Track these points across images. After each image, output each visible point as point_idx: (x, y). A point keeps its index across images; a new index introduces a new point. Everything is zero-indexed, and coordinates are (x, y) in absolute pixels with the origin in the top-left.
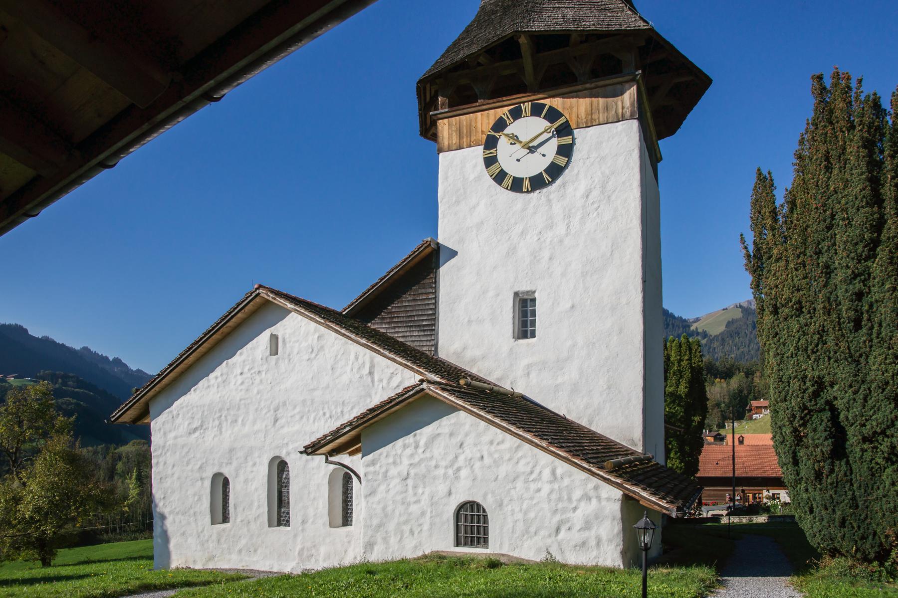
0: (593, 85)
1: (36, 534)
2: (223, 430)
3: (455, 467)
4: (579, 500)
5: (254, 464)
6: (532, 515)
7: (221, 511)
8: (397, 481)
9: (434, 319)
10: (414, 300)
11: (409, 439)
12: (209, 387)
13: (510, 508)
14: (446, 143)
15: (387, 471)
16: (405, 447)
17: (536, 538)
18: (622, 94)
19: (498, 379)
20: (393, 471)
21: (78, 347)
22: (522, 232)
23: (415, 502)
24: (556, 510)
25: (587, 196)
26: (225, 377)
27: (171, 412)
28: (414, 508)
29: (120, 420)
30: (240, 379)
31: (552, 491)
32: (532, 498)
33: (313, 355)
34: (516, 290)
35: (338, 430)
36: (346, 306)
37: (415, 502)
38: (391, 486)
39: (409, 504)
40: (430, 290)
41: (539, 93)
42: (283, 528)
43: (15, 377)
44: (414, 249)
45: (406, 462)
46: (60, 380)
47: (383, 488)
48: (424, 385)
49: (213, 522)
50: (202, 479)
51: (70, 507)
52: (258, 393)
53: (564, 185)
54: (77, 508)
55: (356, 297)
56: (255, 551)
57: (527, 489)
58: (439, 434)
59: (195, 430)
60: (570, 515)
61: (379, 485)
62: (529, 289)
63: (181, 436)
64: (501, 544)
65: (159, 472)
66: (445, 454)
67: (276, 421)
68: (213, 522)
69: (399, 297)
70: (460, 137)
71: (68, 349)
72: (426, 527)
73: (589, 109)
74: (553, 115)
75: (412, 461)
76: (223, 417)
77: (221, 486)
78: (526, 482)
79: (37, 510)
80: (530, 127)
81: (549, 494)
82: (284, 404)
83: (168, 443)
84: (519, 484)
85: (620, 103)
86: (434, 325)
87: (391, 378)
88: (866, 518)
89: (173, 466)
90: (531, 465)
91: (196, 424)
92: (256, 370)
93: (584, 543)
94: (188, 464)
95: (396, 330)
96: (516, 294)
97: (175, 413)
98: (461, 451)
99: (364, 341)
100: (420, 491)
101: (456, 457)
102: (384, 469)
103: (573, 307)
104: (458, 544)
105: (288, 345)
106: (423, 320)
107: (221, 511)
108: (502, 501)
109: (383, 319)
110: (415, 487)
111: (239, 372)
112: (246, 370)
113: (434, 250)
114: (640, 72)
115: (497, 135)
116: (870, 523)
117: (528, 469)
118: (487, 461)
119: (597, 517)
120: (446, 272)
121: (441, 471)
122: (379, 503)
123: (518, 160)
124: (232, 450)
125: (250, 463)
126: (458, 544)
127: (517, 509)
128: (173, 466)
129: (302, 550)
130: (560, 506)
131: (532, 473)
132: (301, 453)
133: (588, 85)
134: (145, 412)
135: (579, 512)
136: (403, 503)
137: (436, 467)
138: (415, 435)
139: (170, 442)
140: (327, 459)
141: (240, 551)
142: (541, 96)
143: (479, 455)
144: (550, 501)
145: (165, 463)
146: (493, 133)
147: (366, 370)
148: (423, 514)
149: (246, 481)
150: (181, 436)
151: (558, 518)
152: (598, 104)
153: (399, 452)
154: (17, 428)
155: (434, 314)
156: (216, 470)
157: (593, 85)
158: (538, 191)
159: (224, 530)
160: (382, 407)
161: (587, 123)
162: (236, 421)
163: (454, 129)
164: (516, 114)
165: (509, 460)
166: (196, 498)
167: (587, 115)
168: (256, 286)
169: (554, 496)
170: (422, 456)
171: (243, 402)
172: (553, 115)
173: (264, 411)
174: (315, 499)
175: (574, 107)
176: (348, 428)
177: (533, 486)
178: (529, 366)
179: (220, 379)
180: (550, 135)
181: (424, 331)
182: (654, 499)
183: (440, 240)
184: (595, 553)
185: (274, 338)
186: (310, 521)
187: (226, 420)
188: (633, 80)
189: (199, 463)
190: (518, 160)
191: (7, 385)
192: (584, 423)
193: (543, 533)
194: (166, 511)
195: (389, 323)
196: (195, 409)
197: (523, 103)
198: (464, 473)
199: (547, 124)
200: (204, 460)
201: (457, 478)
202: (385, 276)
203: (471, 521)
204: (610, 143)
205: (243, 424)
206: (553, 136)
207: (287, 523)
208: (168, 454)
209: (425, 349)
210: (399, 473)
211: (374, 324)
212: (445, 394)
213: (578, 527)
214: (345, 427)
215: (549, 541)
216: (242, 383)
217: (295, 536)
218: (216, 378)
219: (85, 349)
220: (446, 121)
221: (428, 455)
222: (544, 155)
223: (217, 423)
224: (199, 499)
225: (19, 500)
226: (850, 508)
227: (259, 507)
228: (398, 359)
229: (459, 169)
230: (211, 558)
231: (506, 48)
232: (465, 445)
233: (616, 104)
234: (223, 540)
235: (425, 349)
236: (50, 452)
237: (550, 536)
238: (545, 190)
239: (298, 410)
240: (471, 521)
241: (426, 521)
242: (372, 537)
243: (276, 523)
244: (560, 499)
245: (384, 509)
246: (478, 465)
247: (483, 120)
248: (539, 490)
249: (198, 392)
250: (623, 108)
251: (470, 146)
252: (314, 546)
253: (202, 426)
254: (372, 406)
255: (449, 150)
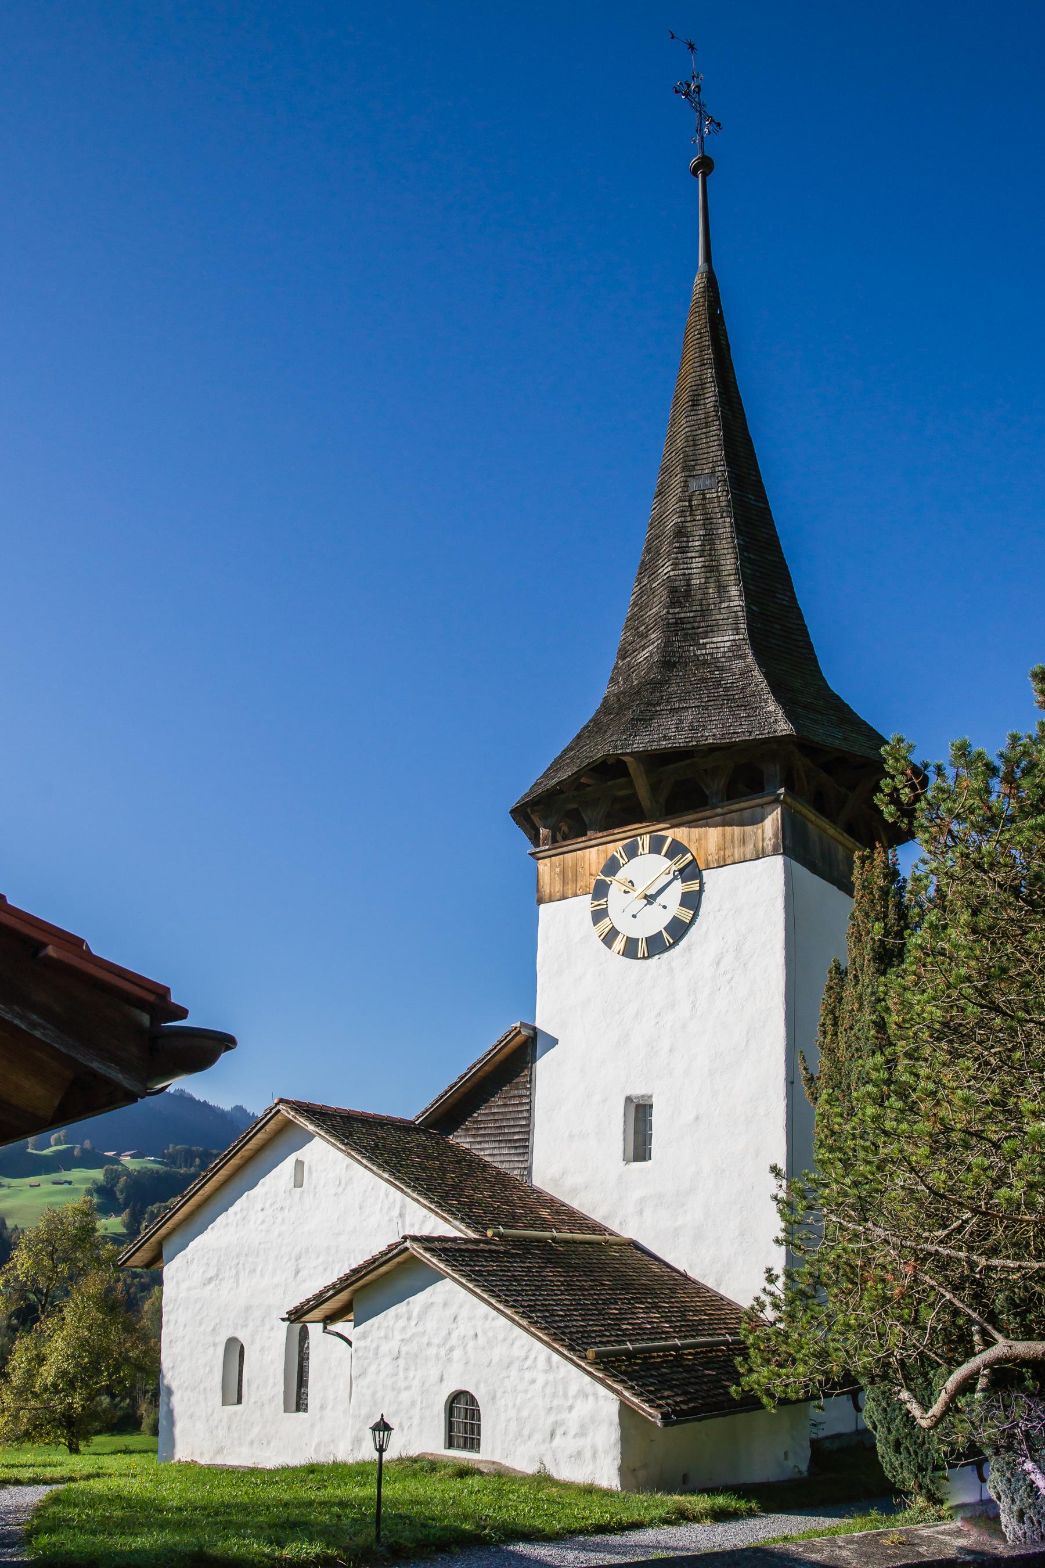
0: (725, 810)
1: (60, 1408)
2: (241, 1282)
3: (448, 1346)
4: (575, 1397)
5: (272, 1329)
6: (525, 1413)
7: (234, 1392)
8: (387, 1360)
9: (528, 1133)
10: (505, 1105)
11: (400, 1308)
12: (227, 1224)
13: (503, 1402)
14: (548, 891)
15: (378, 1347)
16: (397, 1317)
17: (530, 1443)
18: (762, 820)
19: (604, 1218)
20: (384, 1348)
21: (227, 1106)
22: (637, 1014)
23: (406, 1388)
24: (551, 1408)
25: (718, 964)
26: (244, 1213)
27: (186, 1255)
28: (405, 1396)
29: (128, 1264)
30: (261, 1216)
31: (546, 1384)
32: (526, 1391)
33: (340, 1189)
34: (628, 1094)
35: (321, 1293)
36: (419, 1112)
37: (406, 1388)
38: (382, 1366)
39: (399, 1391)
40: (524, 1092)
41: (659, 822)
42: (301, 1414)
43: (133, 1156)
44: (499, 1038)
45: (398, 1336)
46: (197, 1161)
47: (373, 1368)
48: (408, 1244)
49: (224, 1403)
50: (215, 1345)
51: (101, 1372)
52: (279, 1236)
53: (689, 948)
54: (110, 1375)
55: (431, 1101)
56: (268, 1443)
57: (522, 1379)
58: (432, 1303)
59: (211, 1280)
60: (565, 1415)
61: (370, 1364)
62: (643, 1092)
63: (195, 1288)
64: (493, 1448)
65: (169, 1334)
66: (438, 1329)
67: (297, 1272)
68: (224, 1403)
69: (487, 1101)
70: (564, 883)
71: (212, 1109)
72: (416, 1421)
73: (722, 842)
74: (677, 850)
75: (403, 1337)
76: (241, 1266)
77: (235, 1352)
78: (521, 1370)
79: (64, 1374)
80: (649, 869)
81: (544, 1387)
82: (307, 1250)
83: (181, 1295)
84: (514, 1372)
85: (760, 831)
86: (527, 1140)
87: (423, 1222)
88: (924, 1443)
89: (185, 1326)
90: (526, 1348)
91: (211, 1273)
92: (278, 1205)
93: (579, 1454)
94: (200, 1324)
95: (483, 1145)
96: (629, 1099)
97: (189, 1257)
98: (454, 1326)
99: (386, 1175)
100: (411, 1374)
101: (449, 1334)
102: (374, 1345)
103: (697, 1118)
104: (450, 1444)
105: (314, 1175)
106: (515, 1133)
107: (234, 1392)
108: (495, 1392)
109: (467, 1130)
110: (407, 1369)
111: (259, 1209)
112: (267, 1206)
113: (528, 1038)
114: (782, 790)
115: (608, 879)
116: (929, 1450)
117: (523, 1354)
118: (481, 1339)
119: (593, 1420)
120: (544, 1067)
121: (432, 1351)
122: (368, 1387)
123: (634, 916)
124: (248, 1308)
125: (268, 1327)
126: (450, 1444)
127: (510, 1405)
128: (185, 1326)
129: (319, 1444)
130: (555, 1403)
131: (526, 1358)
132: (283, 1320)
133: (719, 810)
134: (157, 1259)
135: (574, 1412)
136: (393, 1389)
137: (429, 1344)
138: (408, 1303)
139: (182, 1295)
140: (325, 1328)
141: (252, 1442)
142: (662, 826)
143: (472, 1333)
144: (544, 1396)
145: (176, 1322)
146: (603, 877)
147: (396, 1213)
148: (413, 1404)
149: (262, 1350)
150: (195, 1288)
151: (552, 1418)
152: (733, 835)
153: (391, 1323)
154: (47, 1262)
155: (528, 1125)
156: (230, 1335)
157: (725, 810)
158: (657, 957)
159: (235, 1413)
160: (365, 1267)
161: (718, 861)
162: (254, 1270)
163: (558, 870)
164: (632, 852)
165: (504, 1340)
166: (208, 1369)
167: (719, 850)
168: (276, 1101)
169: (549, 1390)
170: (414, 1330)
171: (262, 1246)
172: (677, 850)
173: (286, 1259)
174: (335, 1377)
175: (705, 839)
176: (331, 1292)
177: (528, 1376)
178: (642, 1200)
179: (239, 1216)
180: (671, 876)
181: (516, 1147)
182: (636, 1401)
183: (538, 1024)
184: (590, 1468)
185: (299, 1164)
186: (330, 1407)
187: (244, 1269)
188: (777, 800)
189: (213, 1324)
190: (634, 916)
191: (120, 1168)
192: (710, 1283)
193: (538, 1437)
194: (174, 1386)
195: (474, 1136)
196: (211, 1253)
197: (640, 835)
198: (457, 1354)
199: (668, 863)
200: (218, 1320)
201: (450, 1360)
202: (466, 1074)
203: (462, 1416)
204: (752, 888)
205: (262, 1276)
206: (675, 878)
207: (305, 1410)
208: (180, 1310)
209: (516, 1172)
210: (390, 1351)
211: (457, 1136)
212: (428, 1255)
213: (572, 1433)
214: (328, 1291)
215: (543, 1448)
216: (263, 1222)
217: (313, 1426)
218: (236, 1214)
219: (239, 1109)
220: (547, 861)
221: (420, 1329)
222: (665, 907)
223: (233, 1272)
224: (211, 1371)
225: (43, 1360)
226: (905, 1426)
227: (275, 1384)
228: (421, 1200)
229: (562, 926)
230: (220, 1451)
231: (611, 769)
232: (458, 1319)
233: (755, 833)
234: (233, 1427)
235: (516, 1172)
236: (82, 1294)
237: (544, 1441)
238: (666, 955)
239: (321, 1259)
240: (462, 1416)
241: (416, 1412)
242: (360, 1430)
243: (294, 1408)
244: (554, 1395)
245: (374, 1394)
246: (471, 1344)
247: (592, 857)
248: (533, 1381)
249: (215, 1230)
250: (763, 840)
251: (576, 895)
252: (333, 1441)
253: (217, 1275)
254: (354, 1266)
255: (550, 901)
